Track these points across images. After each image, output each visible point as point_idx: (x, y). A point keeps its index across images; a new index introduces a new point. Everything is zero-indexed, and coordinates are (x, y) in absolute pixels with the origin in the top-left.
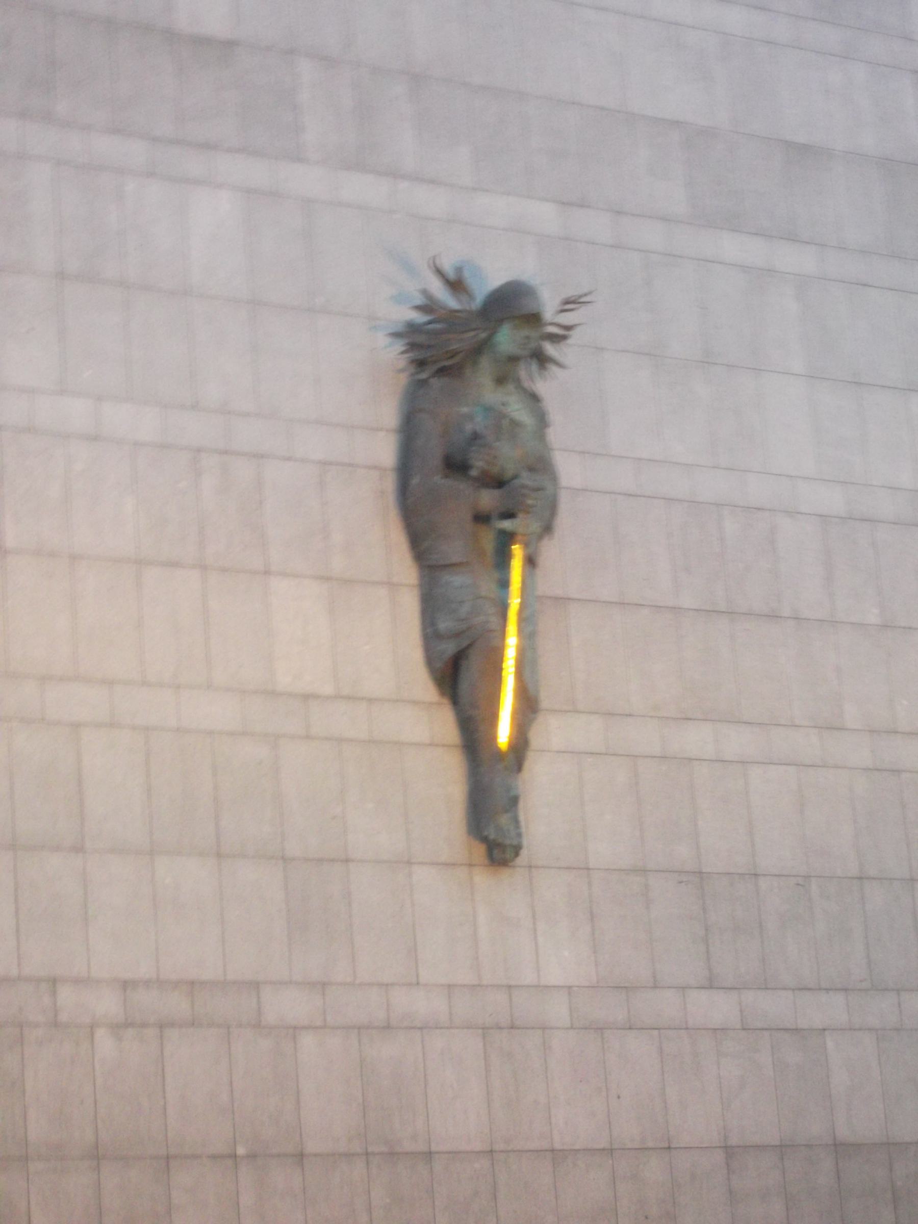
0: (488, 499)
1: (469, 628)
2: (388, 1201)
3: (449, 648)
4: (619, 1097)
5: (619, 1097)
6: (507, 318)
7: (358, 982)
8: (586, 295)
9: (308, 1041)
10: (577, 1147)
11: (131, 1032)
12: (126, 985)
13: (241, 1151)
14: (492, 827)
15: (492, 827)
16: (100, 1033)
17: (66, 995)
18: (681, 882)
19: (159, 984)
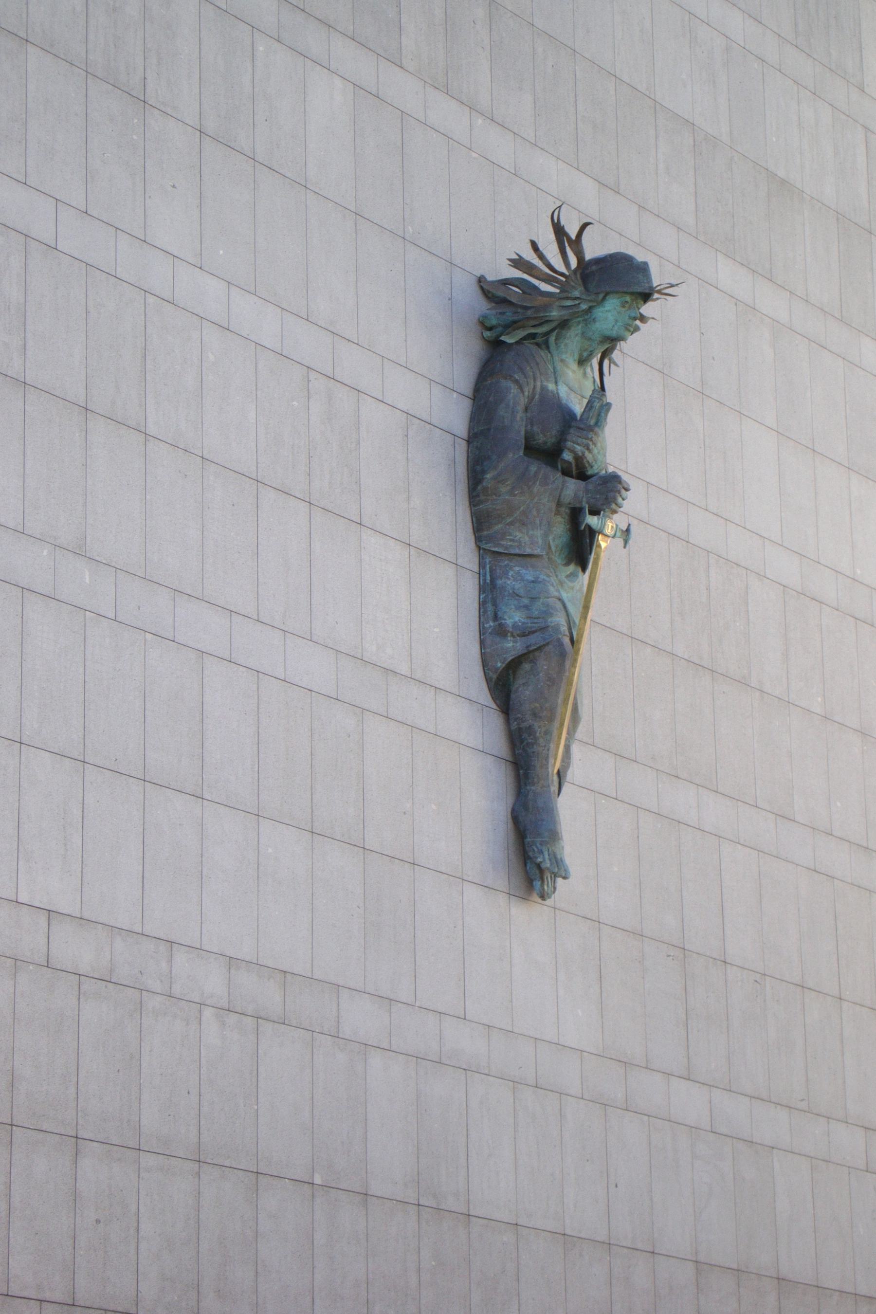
0: (572, 488)
1: (544, 629)
2: (433, 1263)
3: (512, 647)
4: (616, 1186)
5: (616, 1186)
6: (617, 292)
7: (417, 1004)
8: (672, 286)
9: (376, 1060)
10: (583, 1235)
11: (232, 1019)
12: (232, 962)
13: (318, 1180)
14: (530, 853)
15: (530, 853)
16: (208, 1013)
17: (180, 958)
18: (669, 956)
19: (255, 965)
